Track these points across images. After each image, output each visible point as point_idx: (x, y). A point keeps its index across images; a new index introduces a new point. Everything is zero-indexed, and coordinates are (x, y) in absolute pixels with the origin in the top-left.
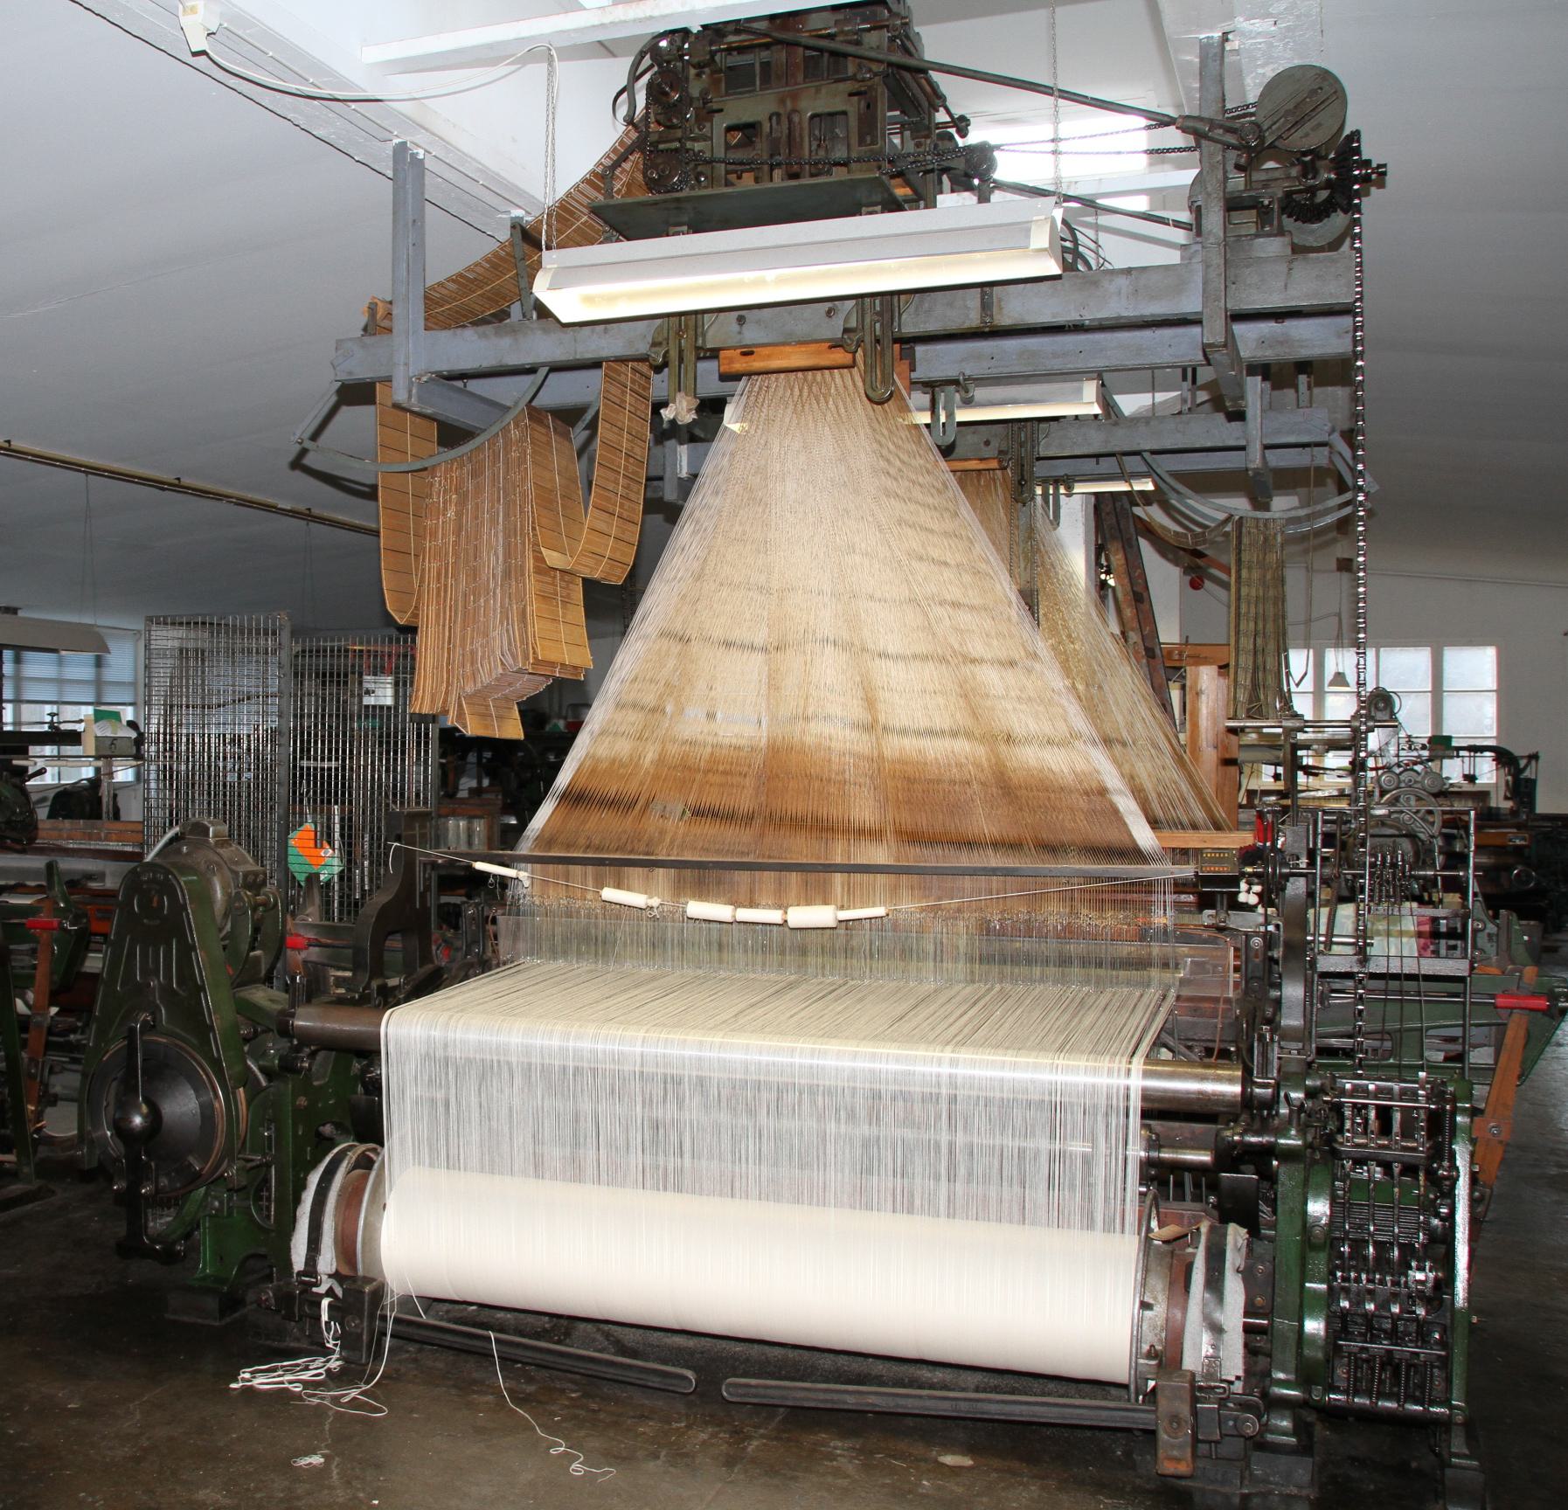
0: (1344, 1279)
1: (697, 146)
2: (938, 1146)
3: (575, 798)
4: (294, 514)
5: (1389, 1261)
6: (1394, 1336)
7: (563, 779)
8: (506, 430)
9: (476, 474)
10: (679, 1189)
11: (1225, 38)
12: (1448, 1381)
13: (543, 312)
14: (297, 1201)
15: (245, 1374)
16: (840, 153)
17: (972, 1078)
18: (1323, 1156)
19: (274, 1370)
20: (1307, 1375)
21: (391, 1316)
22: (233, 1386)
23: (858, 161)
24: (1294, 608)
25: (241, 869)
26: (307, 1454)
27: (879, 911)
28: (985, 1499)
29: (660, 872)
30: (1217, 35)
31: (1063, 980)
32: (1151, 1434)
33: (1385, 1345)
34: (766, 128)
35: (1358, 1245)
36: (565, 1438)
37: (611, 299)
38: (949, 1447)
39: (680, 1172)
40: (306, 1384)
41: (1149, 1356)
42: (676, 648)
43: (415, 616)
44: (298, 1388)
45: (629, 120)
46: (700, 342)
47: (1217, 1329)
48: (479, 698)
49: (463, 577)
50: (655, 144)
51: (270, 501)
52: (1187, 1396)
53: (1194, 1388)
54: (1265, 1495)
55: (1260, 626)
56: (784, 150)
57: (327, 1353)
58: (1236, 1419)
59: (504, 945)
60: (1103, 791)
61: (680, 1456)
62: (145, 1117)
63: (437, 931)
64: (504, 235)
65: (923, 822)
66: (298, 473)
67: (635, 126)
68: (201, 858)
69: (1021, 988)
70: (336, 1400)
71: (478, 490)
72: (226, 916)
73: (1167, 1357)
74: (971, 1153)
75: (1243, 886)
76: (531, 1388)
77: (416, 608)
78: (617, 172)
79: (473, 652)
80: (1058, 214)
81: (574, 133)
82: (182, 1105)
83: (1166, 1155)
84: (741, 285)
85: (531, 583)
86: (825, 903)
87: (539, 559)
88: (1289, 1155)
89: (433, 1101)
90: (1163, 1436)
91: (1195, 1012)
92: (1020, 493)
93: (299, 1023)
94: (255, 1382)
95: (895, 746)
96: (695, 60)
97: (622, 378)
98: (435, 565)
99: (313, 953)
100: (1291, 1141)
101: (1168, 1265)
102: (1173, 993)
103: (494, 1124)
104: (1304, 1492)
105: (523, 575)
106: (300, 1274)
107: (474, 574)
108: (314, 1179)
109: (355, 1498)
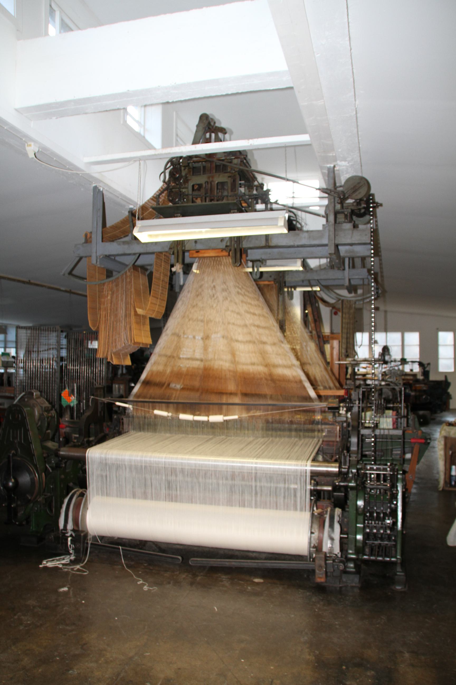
0: (368, 523)
1: (184, 190)
2: (252, 486)
3: (147, 383)
4: (66, 291)
5: (380, 517)
6: (382, 539)
8: (126, 273)
9: (117, 285)
10: (176, 501)
11: (334, 167)
12: (396, 551)
13: (136, 238)
14: (61, 507)
15: (44, 562)
16: (225, 193)
17: (262, 467)
18: (361, 488)
20: (359, 551)
21: (90, 542)
22: (41, 566)
23: (230, 196)
25: (44, 406)
27: (236, 417)
28: (266, 592)
29: (171, 405)
30: (332, 166)
31: (290, 437)
32: (314, 571)
33: (379, 542)
34: (204, 186)
35: (371, 514)
36: (143, 578)
37: (157, 236)
38: (256, 577)
39: (176, 496)
40: (63, 564)
41: (313, 547)
42: (176, 339)
43: (98, 328)
44: (61, 566)
45: (164, 181)
46: (183, 248)
47: (332, 539)
48: (117, 354)
49: (112, 317)
50: (171, 189)
51: (58, 287)
52: (323, 559)
53: (326, 556)
54: (346, 586)
55: (348, 331)
56: (209, 192)
57: (70, 554)
58: (337, 565)
59: (125, 426)
60: (301, 381)
61: (177, 583)
62: (13, 483)
63: (105, 423)
64: (127, 213)
65: (248, 391)
66: (70, 276)
67: (166, 183)
68: (32, 402)
69: (278, 439)
70: (72, 569)
71: (117, 291)
72: (39, 420)
73: (318, 548)
75: (341, 409)
76: (132, 563)
77: (99, 326)
78: (161, 196)
79: (115, 340)
80: (287, 216)
81: (147, 185)
82: (25, 479)
83: (319, 488)
84: (195, 233)
85: (133, 318)
86: (221, 414)
87: (135, 312)
88: (352, 488)
89: (102, 476)
90: (317, 571)
91: (328, 445)
92: (280, 291)
93: (62, 453)
95: (240, 368)
96: (183, 165)
97: (161, 258)
98: (104, 313)
99: (68, 430)
100: (352, 484)
101: (318, 521)
102: (321, 440)
103: (121, 483)
104: (357, 585)
105: (130, 316)
106: (62, 530)
107: (116, 316)
108: (66, 501)
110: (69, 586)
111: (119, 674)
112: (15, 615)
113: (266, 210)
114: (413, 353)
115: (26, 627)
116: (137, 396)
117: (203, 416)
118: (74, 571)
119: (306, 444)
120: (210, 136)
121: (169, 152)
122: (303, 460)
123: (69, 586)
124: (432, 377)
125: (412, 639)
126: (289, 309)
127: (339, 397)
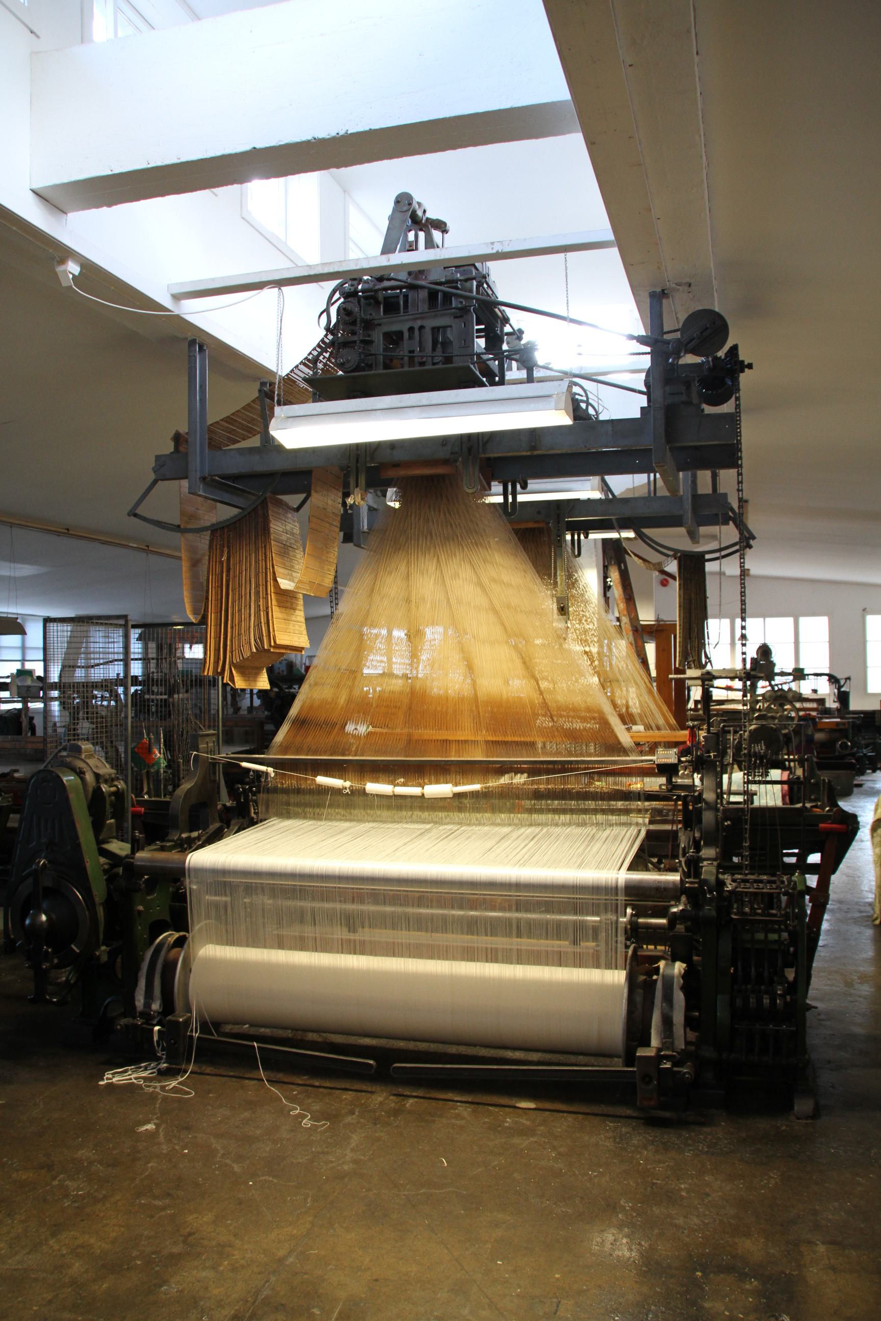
3: (301, 723)
7: (294, 711)
15: (108, 1075)
19: (126, 1071)
22: (101, 1083)
24: (712, 603)
26: (144, 1124)
28: (542, 1128)
40: (145, 1079)
45: (328, 329)
57: (158, 1059)
74: (530, 928)
81: (284, 333)
94: (114, 1080)
109: (174, 1149)
110: (156, 1121)
111: (258, 1292)
112: (54, 1178)
113: (530, 379)
114: (816, 656)
115: (75, 1201)
116: (285, 749)
117: (412, 786)
118: (167, 1091)
119: (615, 838)
120: (416, 236)
121: (336, 270)
122: (609, 869)
123: (156, 1121)
124: (855, 705)
125: (830, 1217)
126: (580, 573)
127: (675, 744)
